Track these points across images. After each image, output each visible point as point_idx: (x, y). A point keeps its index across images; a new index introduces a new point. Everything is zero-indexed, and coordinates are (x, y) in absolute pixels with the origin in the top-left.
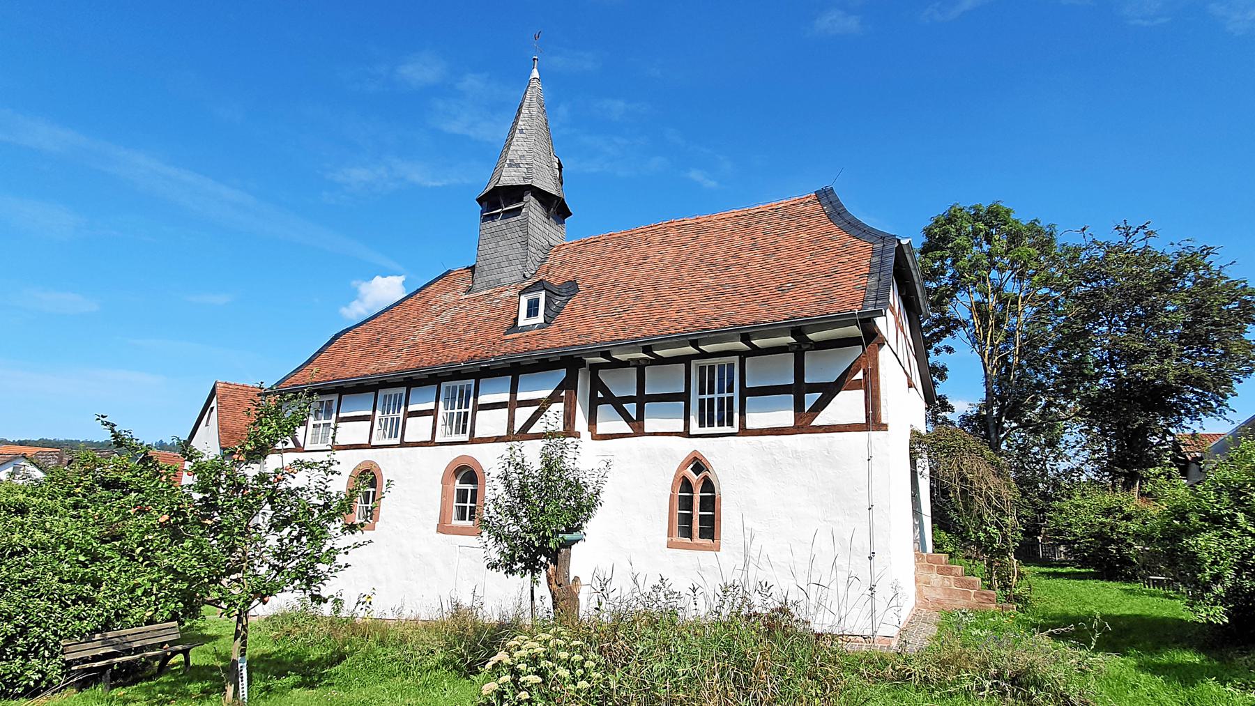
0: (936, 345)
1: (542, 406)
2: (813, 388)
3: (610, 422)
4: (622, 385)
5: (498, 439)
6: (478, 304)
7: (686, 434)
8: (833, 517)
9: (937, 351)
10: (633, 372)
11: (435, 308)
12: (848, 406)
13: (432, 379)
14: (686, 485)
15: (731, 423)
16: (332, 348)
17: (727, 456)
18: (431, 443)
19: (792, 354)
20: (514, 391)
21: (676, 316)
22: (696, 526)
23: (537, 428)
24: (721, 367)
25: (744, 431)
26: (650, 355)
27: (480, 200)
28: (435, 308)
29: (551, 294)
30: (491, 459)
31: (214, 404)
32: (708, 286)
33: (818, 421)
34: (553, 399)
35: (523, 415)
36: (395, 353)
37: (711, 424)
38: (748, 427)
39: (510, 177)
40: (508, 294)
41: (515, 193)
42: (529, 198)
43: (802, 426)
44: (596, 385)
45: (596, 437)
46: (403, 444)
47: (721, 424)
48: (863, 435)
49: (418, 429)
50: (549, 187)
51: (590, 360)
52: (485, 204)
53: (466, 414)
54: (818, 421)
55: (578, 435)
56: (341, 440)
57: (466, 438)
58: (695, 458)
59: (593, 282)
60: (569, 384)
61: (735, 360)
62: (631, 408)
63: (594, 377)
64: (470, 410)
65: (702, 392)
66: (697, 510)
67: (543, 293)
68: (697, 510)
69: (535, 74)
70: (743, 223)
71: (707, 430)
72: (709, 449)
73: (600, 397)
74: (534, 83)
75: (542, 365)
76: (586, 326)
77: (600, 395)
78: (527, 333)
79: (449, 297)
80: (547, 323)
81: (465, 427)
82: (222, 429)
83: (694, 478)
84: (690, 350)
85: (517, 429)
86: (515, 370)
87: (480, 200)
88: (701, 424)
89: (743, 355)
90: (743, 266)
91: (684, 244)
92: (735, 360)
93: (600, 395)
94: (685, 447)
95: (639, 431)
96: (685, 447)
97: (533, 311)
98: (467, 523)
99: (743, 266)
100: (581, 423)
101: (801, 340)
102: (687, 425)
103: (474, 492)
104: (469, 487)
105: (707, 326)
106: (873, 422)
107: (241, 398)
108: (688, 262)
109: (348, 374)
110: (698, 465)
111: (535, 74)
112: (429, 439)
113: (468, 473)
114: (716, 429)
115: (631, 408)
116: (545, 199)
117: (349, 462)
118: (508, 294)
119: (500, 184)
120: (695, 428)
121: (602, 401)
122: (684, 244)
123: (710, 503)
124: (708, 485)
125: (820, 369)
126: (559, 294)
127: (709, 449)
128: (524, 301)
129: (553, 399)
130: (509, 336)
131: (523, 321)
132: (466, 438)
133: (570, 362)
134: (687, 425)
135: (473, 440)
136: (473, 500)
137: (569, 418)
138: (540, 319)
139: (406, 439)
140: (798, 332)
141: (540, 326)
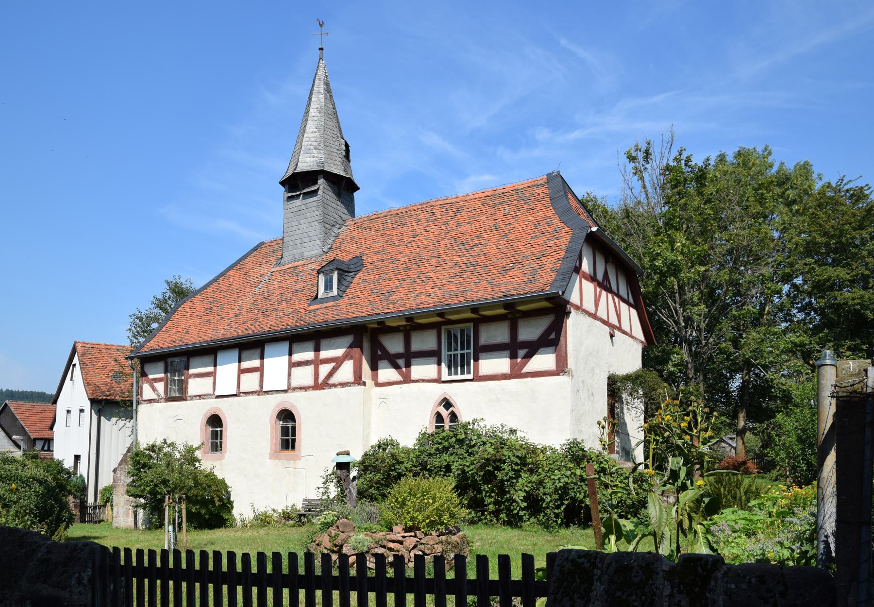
1: (338, 362)
3: (387, 373)
4: (394, 345)
5: (305, 388)
7: (439, 381)
11: (253, 280)
12: (544, 360)
14: (439, 418)
15: (469, 373)
20: (407, 344)
21: (430, 291)
23: (334, 380)
24: (462, 331)
25: (477, 378)
26: (411, 325)
27: (283, 183)
28: (253, 280)
31: (76, 360)
33: (526, 369)
34: (346, 357)
35: (325, 369)
39: (306, 163)
42: (321, 181)
43: (516, 373)
45: (378, 385)
50: (337, 169)
55: (364, 384)
61: (471, 325)
62: (401, 362)
65: (449, 349)
69: (834, 554)
70: (491, 203)
72: (453, 391)
76: (360, 304)
77: (379, 353)
82: (87, 384)
83: (445, 413)
86: (316, 336)
87: (283, 183)
88: (450, 374)
92: (471, 325)
93: (379, 353)
95: (407, 379)
97: (328, 286)
101: (512, 311)
102: (440, 372)
103: (294, 428)
104: (290, 425)
106: (561, 368)
108: (446, 241)
109: (192, 341)
110: (447, 404)
111: (834, 554)
114: (460, 377)
115: (401, 362)
116: (334, 180)
119: (298, 170)
120: (445, 376)
121: (382, 358)
125: (529, 332)
126: (344, 271)
127: (453, 391)
129: (346, 357)
130: (312, 308)
134: (440, 372)
136: (294, 434)
138: (335, 292)
139: (242, 390)
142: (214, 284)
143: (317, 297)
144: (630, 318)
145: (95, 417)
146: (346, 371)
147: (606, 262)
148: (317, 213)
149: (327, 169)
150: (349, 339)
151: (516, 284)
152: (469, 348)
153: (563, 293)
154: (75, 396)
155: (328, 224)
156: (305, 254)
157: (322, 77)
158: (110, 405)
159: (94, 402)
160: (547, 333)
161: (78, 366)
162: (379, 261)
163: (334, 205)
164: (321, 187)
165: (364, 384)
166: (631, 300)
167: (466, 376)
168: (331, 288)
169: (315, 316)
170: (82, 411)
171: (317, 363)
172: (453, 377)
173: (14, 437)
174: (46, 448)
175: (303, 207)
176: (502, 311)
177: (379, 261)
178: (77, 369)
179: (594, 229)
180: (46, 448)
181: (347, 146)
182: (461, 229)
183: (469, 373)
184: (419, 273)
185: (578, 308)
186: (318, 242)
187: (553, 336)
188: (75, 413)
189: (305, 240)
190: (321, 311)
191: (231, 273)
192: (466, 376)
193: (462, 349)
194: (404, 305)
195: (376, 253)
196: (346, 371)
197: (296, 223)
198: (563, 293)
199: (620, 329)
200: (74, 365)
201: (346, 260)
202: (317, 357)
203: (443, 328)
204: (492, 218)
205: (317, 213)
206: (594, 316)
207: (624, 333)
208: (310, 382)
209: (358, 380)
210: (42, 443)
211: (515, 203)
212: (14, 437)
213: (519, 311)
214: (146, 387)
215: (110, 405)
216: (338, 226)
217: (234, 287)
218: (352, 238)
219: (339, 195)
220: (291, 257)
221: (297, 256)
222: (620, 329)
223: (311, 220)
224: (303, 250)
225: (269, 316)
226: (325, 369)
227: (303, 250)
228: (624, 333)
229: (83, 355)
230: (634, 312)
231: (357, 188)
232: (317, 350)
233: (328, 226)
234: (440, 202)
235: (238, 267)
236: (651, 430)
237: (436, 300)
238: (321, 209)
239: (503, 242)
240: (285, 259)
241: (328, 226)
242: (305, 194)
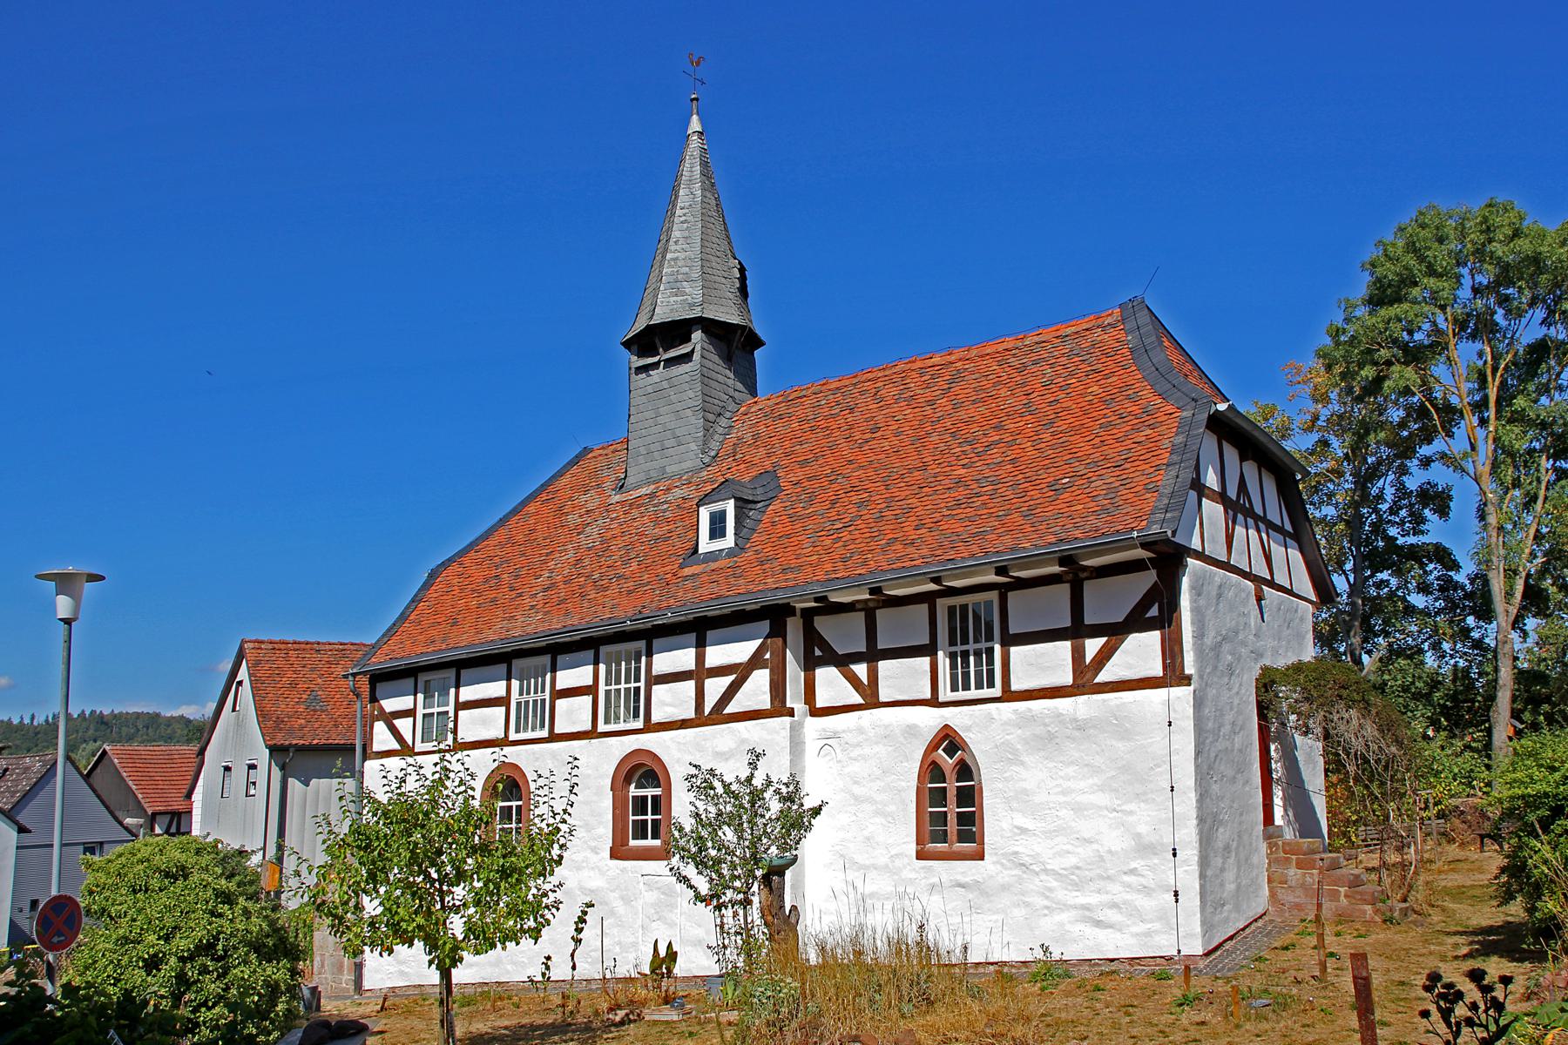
0: (1425, 450)
1: (741, 673)
2: (1096, 631)
3: (831, 684)
4: (844, 634)
6: (635, 513)
7: (934, 702)
8: (1105, 815)
9: (1426, 462)
10: (859, 619)
11: (573, 519)
13: (588, 646)
15: (991, 685)
16: (432, 594)
17: (986, 728)
18: (591, 734)
19: (1067, 586)
22: (952, 826)
29: (743, 504)
30: (678, 752)
31: (243, 674)
32: (960, 481)
33: (1102, 677)
34: (755, 662)
35: (715, 688)
36: (527, 601)
37: (966, 687)
38: (1014, 687)
39: (667, 309)
40: (678, 493)
41: (676, 332)
42: (697, 336)
43: (1084, 681)
44: (812, 638)
45: (816, 712)
46: (554, 737)
47: (979, 686)
48: (1160, 694)
49: (575, 713)
51: (799, 606)
52: (635, 348)
53: (637, 690)
54: (1102, 677)
55: (791, 713)
56: (466, 735)
57: (639, 724)
58: (946, 736)
59: (800, 474)
60: (778, 631)
63: (810, 630)
64: (642, 684)
66: (950, 808)
67: (732, 501)
68: (950, 808)
69: (695, 124)
71: (962, 695)
73: (817, 654)
74: (695, 142)
75: (732, 621)
77: (818, 652)
78: (713, 565)
79: (591, 500)
80: (739, 547)
81: (637, 710)
83: (947, 762)
84: (933, 587)
85: (707, 711)
86: (701, 629)
88: (954, 688)
89: (1003, 590)
90: (1009, 445)
91: (931, 403)
92: (993, 596)
93: (818, 652)
94: (931, 720)
95: (871, 699)
96: (931, 720)
97: (717, 531)
98: (650, 842)
99: (1009, 445)
100: (794, 700)
104: (650, 792)
105: (951, 554)
107: (281, 663)
108: (935, 438)
111: (695, 124)
112: (588, 726)
113: (642, 771)
114: (973, 693)
116: (718, 332)
117: (482, 763)
118: (678, 493)
119: (656, 320)
122: (931, 403)
123: (969, 796)
124: (965, 771)
125: (1109, 600)
128: (704, 514)
130: (687, 571)
131: (705, 545)
132: (639, 724)
133: (774, 617)
135: (650, 727)
137: (778, 688)
138: (729, 541)
140: (1067, 560)
141: (731, 553)
142: (503, 531)
143: (696, 550)
144: (1291, 565)
145: (277, 773)
146: (757, 689)
147: (1243, 459)
148: (691, 394)
149: (709, 314)
150: (765, 626)
151: (1077, 522)
152: (637, 680)
153: (1174, 533)
154: (241, 739)
155: (711, 414)
156: (668, 469)
157: (696, 153)
158: (304, 755)
159: (275, 750)
160: (1144, 605)
161: (247, 683)
162: (809, 479)
163: (720, 378)
164: (698, 348)
165: (791, 713)
166: (1288, 527)
167: (986, 693)
168: (723, 535)
169: (696, 588)
170: (252, 767)
171: (700, 674)
172: (962, 695)
173: (128, 821)
174: (173, 830)
175: (665, 384)
176: (1056, 569)
177: (809, 479)
178: (246, 691)
179: (1222, 407)
180: (173, 830)
181: (742, 270)
182: (963, 415)
183: (991, 685)
184: (889, 501)
185: (1200, 556)
186: (693, 446)
187: (1154, 611)
188: (239, 774)
189: (668, 444)
190: (705, 578)
191: (532, 508)
192: (986, 693)
193: (976, 641)
194: (865, 563)
195: (804, 464)
196: (757, 689)
197: (652, 414)
198: (1174, 533)
199: (1272, 584)
200: (240, 683)
201: (1260, 901)
202: (700, 659)
203: (942, 604)
204: (1018, 391)
205: (691, 394)
206: (1226, 566)
207: (1281, 588)
208: (690, 713)
209: (779, 708)
210: (167, 819)
211: (1063, 360)
212: (128, 821)
213: (1085, 568)
214: (380, 728)
215: (304, 755)
216: (728, 415)
217: (540, 535)
218: (756, 437)
219: (728, 359)
220: (642, 476)
221: (653, 474)
222: (1272, 584)
223: (679, 406)
224: (664, 462)
225: (606, 588)
226: (715, 688)
227: (664, 462)
228: (1281, 588)
229: (257, 663)
230: (1295, 555)
231: (760, 343)
232: (701, 645)
233: (711, 417)
234: (919, 364)
235: (544, 496)
236: (1334, 766)
237: (925, 552)
238: (698, 386)
239: (1046, 437)
240: (630, 480)
241: (711, 417)
242: (666, 361)
